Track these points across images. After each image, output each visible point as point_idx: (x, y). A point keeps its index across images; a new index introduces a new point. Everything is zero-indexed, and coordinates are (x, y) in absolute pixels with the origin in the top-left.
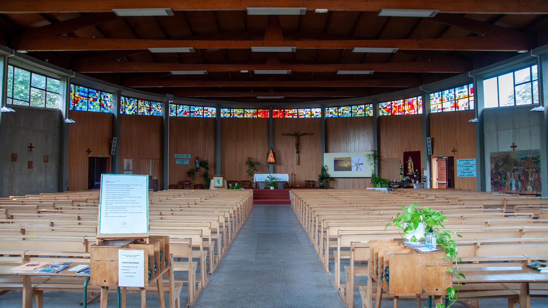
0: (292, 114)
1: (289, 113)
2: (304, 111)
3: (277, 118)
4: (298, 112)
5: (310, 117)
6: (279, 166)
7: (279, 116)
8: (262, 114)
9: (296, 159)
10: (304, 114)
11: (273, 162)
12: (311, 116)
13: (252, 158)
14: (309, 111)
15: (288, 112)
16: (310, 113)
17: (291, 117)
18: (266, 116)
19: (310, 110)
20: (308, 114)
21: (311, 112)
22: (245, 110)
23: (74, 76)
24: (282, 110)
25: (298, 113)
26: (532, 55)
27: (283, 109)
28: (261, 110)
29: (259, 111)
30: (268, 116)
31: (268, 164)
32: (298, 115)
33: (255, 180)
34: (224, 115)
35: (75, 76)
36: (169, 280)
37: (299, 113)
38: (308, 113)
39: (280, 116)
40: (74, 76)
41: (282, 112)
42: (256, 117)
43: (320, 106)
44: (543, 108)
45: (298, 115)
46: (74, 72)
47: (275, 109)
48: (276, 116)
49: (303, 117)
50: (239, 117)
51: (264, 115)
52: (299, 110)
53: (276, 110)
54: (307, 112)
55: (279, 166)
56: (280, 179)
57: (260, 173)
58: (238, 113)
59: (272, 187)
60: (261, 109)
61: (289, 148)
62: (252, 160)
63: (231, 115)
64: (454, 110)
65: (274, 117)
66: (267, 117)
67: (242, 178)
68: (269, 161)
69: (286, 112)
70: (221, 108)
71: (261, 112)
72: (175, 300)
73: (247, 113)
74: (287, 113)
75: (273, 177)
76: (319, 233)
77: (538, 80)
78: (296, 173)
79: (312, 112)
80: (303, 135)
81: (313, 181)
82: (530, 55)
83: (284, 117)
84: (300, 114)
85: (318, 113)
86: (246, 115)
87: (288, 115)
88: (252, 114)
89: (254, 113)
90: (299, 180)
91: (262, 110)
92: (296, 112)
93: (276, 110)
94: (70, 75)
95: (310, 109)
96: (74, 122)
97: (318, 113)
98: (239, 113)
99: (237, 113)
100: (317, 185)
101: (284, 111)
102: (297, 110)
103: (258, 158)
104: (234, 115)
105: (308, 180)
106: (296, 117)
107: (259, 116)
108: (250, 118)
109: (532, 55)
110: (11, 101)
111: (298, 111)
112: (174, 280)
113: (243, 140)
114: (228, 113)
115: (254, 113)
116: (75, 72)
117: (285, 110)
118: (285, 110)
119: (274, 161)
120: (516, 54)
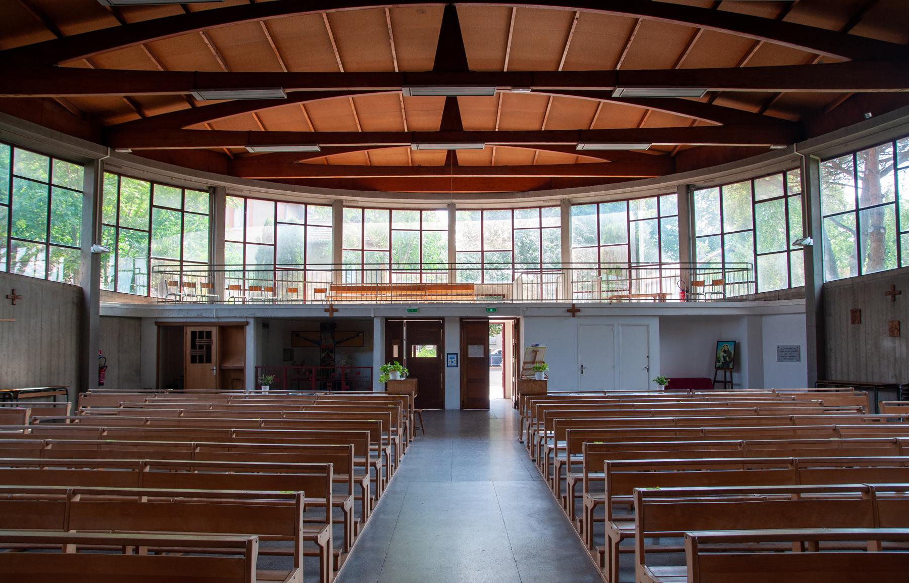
23: (108, 156)
26: (795, 153)
35: (110, 156)
36: (348, 474)
40: (108, 156)
44: (812, 240)
46: (109, 148)
57: (879, 276)
64: (225, 287)
72: (616, 542)
76: (10, 405)
77: (802, 194)
82: (794, 152)
94: (102, 155)
96: (813, 63)
109: (795, 153)
110: (4, 194)
112: (635, 502)
116: (111, 148)
120: (767, 150)
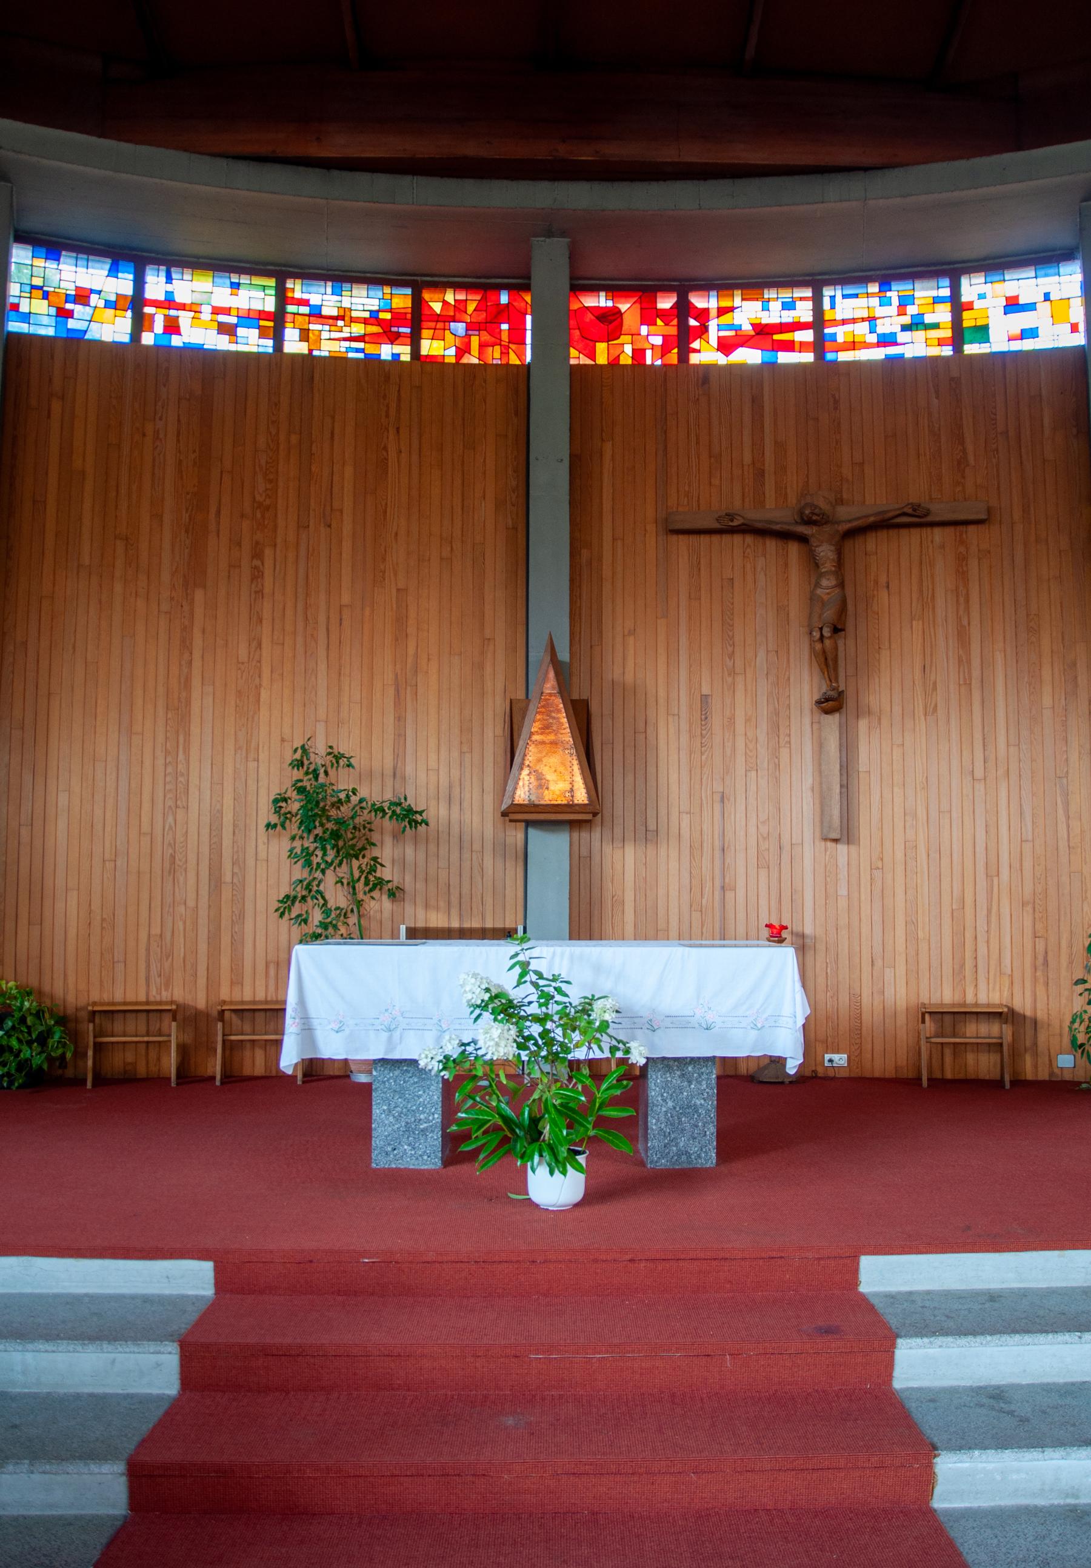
0: (763, 334)
1: (731, 327)
2: (885, 302)
3: (614, 363)
4: (818, 310)
5: (947, 351)
6: (629, 850)
7: (628, 349)
8: (460, 328)
9: (809, 781)
10: (883, 328)
11: (570, 807)
12: (958, 337)
13: (338, 757)
14: (936, 300)
15: (722, 311)
16: (943, 315)
17: (749, 356)
18: (505, 353)
19: (946, 292)
20: (928, 327)
21: (958, 307)
22: (297, 289)
24: (665, 303)
25: (819, 322)
27: (667, 289)
28: (450, 297)
29: (437, 307)
30: (520, 355)
31: (516, 835)
32: (820, 345)
33: (307, 1030)
34: (70, 314)
37: (834, 323)
38: (929, 319)
39: (638, 354)
41: (664, 315)
42: (406, 358)
43: (1061, 235)
45: (820, 345)
47: (594, 289)
48: (601, 347)
49: (878, 354)
50: (223, 343)
51: (482, 346)
52: (828, 292)
53: (602, 301)
54: (912, 310)
55: (629, 850)
56: (681, 1023)
58: (216, 311)
59: (558, 1164)
60: (457, 287)
61: (739, 663)
62: (343, 781)
63: (140, 323)
65: (585, 361)
66: (514, 360)
67: (237, 981)
68: (523, 792)
69: (703, 315)
70: (23, 238)
71: (457, 312)
73: (316, 315)
74: (713, 325)
75: (575, 996)
78: (808, 930)
79: (969, 306)
80: (884, 524)
81: (1007, 1016)
83: (683, 358)
84: (841, 333)
85: (1031, 307)
86: (305, 335)
87: (725, 346)
88: (358, 329)
89: (387, 316)
90: (844, 998)
91: (461, 296)
92: (804, 312)
93: (602, 301)
95: (946, 282)
97: (1031, 307)
98: (227, 311)
99: (206, 310)
100: (1043, 1060)
101: (683, 309)
102: (808, 293)
103: (409, 769)
104: (172, 328)
105: (946, 996)
106: (808, 357)
107: (430, 347)
108: (337, 362)
111: (817, 300)
113: (257, 575)
114: (108, 305)
115: (379, 322)
117: (698, 301)
118: (698, 301)
119: (581, 796)
